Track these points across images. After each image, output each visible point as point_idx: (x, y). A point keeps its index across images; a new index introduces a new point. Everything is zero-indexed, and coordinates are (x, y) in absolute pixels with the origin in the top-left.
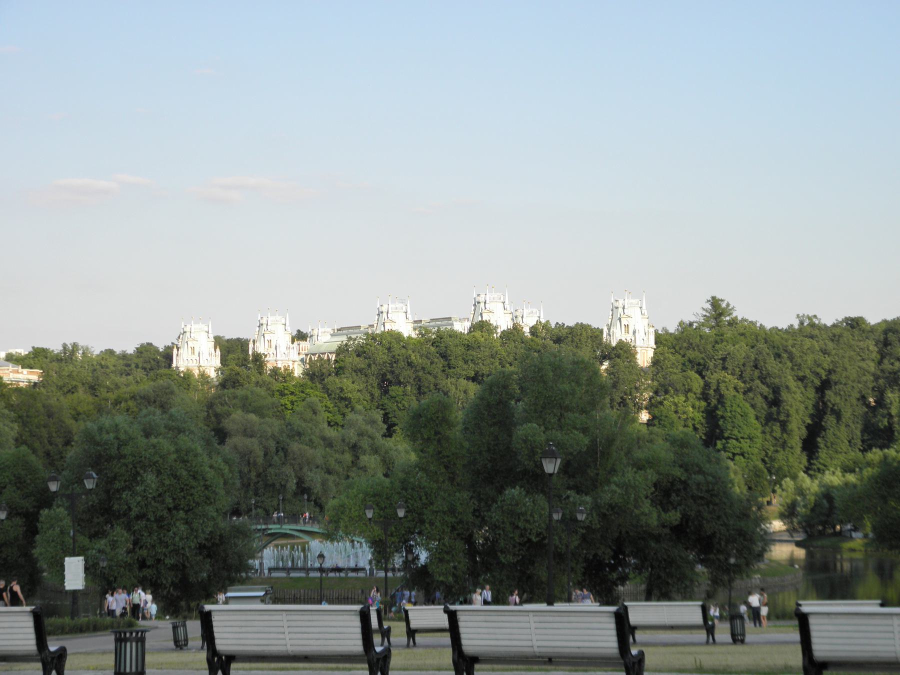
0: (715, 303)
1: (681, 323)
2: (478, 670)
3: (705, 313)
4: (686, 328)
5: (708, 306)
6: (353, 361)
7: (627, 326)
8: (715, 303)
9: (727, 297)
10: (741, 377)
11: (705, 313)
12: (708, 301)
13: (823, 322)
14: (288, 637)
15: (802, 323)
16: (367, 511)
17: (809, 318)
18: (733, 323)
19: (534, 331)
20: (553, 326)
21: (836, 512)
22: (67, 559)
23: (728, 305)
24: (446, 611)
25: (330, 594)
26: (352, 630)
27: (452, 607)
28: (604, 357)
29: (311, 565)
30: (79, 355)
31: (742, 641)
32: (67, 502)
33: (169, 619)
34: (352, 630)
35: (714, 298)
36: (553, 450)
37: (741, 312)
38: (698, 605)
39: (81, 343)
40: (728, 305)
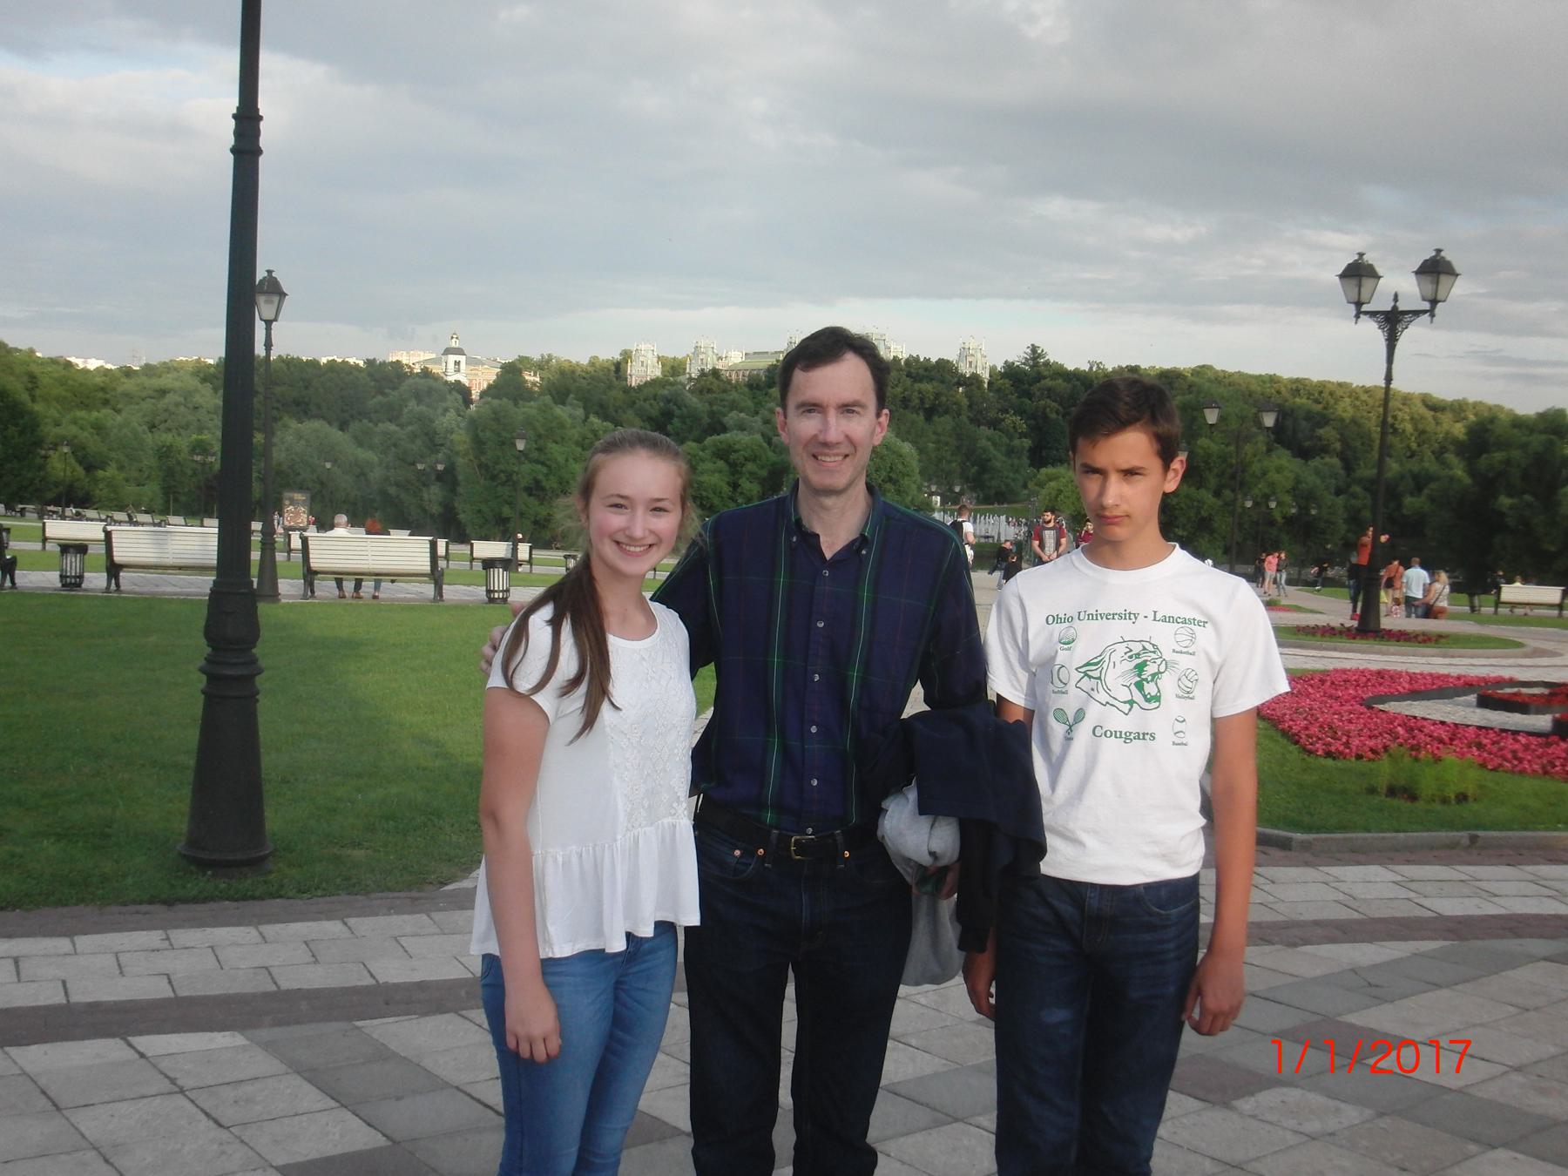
0: (1034, 349)
1: (1006, 362)
2: (201, 569)
3: (1026, 356)
5: (1029, 351)
7: (971, 363)
8: (1034, 349)
9: (1043, 345)
11: (1026, 356)
12: (1028, 347)
13: (1106, 367)
14: (370, 558)
15: (1091, 368)
16: (326, 463)
18: (1047, 364)
19: (907, 361)
20: (922, 360)
21: (1468, 481)
24: (105, 530)
25: (989, 518)
26: (212, 553)
27: (109, 528)
28: (959, 384)
29: (657, 509)
34: (120, 554)
35: (1033, 345)
37: (1053, 357)
40: (1043, 351)
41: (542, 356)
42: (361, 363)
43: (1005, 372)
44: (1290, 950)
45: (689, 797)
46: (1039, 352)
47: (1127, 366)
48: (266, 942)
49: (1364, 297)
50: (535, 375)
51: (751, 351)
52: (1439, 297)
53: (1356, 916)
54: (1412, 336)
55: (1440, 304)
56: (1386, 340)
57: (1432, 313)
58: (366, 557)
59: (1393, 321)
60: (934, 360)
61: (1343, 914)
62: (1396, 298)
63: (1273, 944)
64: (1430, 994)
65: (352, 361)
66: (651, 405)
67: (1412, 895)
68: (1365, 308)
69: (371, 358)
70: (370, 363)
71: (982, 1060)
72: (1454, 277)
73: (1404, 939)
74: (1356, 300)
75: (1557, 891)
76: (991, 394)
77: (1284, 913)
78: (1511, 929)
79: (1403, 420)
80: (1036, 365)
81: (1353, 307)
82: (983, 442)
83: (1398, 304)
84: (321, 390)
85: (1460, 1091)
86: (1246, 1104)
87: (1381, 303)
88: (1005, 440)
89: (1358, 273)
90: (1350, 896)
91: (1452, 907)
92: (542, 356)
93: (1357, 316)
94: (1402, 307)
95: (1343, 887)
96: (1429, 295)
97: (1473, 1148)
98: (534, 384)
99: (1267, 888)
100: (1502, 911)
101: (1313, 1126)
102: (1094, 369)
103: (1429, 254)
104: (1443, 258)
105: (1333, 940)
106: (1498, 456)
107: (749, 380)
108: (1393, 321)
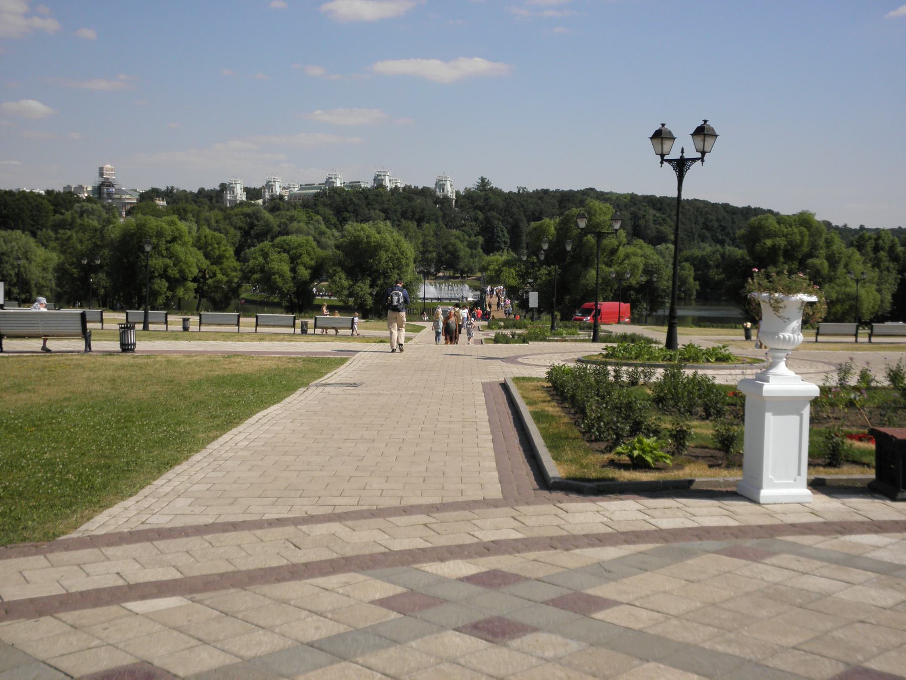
0: (483, 179)
1: (466, 188)
4: (468, 191)
5: (480, 181)
6: (762, 290)
8: (483, 179)
9: (489, 177)
10: (500, 214)
13: (529, 190)
15: (519, 191)
17: (523, 189)
18: (491, 189)
19: (404, 189)
22: (629, 304)
23: (488, 181)
30: (175, 191)
31: (306, 333)
32: (276, 278)
33: (427, 321)
35: (482, 177)
36: (110, 203)
37: (495, 184)
38: (76, 314)
39: (175, 187)
40: (488, 181)
41: (167, 187)
42: (43, 192)
43: (465, 195)
44: (565, 553)
45: (483, 384)
46: (486, 181)
47: (542, 190)
48: (213, 547)
49: (666, 150)
50: (163, 200)
51: (303, 184)
52: (706, 150)
53: (610, 530)
54: (693, 173)
55: (707, 154)
56: (678, 177)
57: (702, 159)
58: (37, 325)
59: (681, 166)
60: (420, 187)
61: (603, 530)
62: (682, 152)
63: (556, 549)
64: (640, 576)
65: (37, 191)
66: (190, 228)
67: (647, 517)
68: (666, 157)
69: (50, 189)
70: (49, 193)
71: (368, 624)
72: (715, 137)
73: (634, 543)
74: (702, 150)
75: (732, 512)
76: (457, 209)
77: (578, 531)
78: (697, 536)
79: (712, 220)
80: (485, 190)
81: (659, 157)
82: (453, 240)
83: (684, 154)
84: (17, 210)
85: (640, 631)
86: (515, 643)
87: (675, 154)
88: (466, 237)
89: (660, 136)
90: (610, 519)
91: (666, 523)
92: (167, 187)
93: (662, 163)
94: (686, 156)
95: (607, 514)
96: (700, 147)
97: (636, 662)
98: (163, 206)
99: (562, 516)
100: (696, 525)
101: (549, 654)
102: (521, 192)
103: (658, 127)
104: (666, 129)
105: (592, 545)
106: (769, 243)
107: (303, 202)
108: (681, 166)
